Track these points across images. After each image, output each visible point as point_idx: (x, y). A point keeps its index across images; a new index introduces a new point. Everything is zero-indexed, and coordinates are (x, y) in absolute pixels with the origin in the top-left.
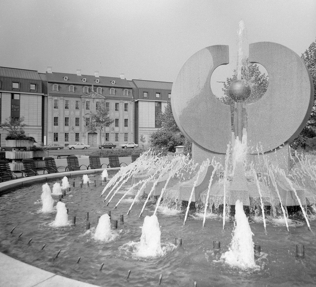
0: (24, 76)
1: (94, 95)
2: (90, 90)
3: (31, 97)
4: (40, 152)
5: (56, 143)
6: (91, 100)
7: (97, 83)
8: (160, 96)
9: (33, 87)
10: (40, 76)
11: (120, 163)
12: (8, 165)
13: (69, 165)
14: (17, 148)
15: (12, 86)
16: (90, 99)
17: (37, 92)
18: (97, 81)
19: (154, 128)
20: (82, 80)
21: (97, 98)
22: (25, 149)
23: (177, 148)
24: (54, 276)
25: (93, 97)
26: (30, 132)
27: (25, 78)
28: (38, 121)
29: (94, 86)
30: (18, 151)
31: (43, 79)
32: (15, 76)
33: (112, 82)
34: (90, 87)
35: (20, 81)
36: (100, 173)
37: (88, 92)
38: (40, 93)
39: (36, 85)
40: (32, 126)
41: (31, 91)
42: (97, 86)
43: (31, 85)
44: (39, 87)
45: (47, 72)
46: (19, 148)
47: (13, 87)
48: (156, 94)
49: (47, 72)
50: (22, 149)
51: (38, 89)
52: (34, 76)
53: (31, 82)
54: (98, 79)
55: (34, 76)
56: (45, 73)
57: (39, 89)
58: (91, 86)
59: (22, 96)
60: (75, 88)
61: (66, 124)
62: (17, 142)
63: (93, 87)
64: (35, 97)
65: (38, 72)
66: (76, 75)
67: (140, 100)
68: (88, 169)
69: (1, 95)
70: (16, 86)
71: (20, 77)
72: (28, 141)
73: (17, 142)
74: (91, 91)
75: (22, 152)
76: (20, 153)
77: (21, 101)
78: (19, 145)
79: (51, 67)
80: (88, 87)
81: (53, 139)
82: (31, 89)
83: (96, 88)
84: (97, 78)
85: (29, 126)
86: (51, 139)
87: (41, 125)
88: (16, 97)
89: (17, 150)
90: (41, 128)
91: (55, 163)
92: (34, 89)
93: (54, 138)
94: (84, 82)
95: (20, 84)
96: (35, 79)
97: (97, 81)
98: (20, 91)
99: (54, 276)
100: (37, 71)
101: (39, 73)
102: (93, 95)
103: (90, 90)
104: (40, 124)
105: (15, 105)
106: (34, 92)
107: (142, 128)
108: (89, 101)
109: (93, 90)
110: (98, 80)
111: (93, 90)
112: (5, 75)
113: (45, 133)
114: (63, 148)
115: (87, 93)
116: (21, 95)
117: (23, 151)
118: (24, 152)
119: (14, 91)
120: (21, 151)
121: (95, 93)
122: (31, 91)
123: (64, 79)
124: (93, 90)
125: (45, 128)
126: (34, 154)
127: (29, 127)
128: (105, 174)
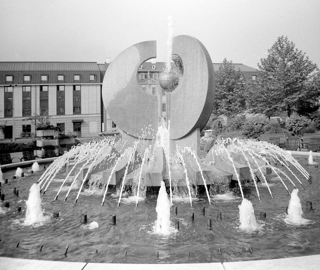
0: (68, 68)
1: (150, 81)
2: (146, 77)
3: (91, 87)
4: (67, 139)
5: (114, 129)
6: (147, 86)
7: (153, 69)
8: (95, 78)
9: (92, 78)
10: (99, 67)
11: (12, 158)
12: (54, 151)
13: (24, 156)
14: (44, 137)
15: (74, 78)
16: (146, 85)
17: (96, 82)
18: (154, 67)
19: (72, 115)
20: (151, 67)
21: (153, 84)
22: (52, 137)
23: (206, 133)
24: (86, 265)
25: (149, 83)
26: (90, 120)
27: (85, 70)
28: (98, 109)
29: (151, 72)
30: (46, 140)
31: (102, 70)
32: (77, 70)
33: (152, 67)
34: (146, 73)
35: (81, 74)
36: (30, 165)
37: (144, 79)
38: (99, 83)
39: (95, 75)
40: (85, 114)
41: (90, 81)
42: (153, 72)
43: (91, 76)
44: (97, 77)
45: (105, 62)
46: (47, 137)
47: (75, 79)
48: (89, 76)
49: (105, 62)
50: (49, 138)
51: (96, 79)
52: (93, 68)
53: (42, 73)
54: (154, 65)
55: (93, 68)
56: (104, 63)
57: (97, 79)
58: (147, 72)
59: (50, 88)
60: (145, 75)
61: (163, 110)
62: (44, 132)
63: (148, 74)
64: (94, 87)
65: (98, 63)
66: (151, 63)
67: (51, 84)
68: (21, 161)
69: (65, 87)
70: (77, 78)
71: (81, 70)
72: (54, 130)
73: (44, 132)
74: (147, 78)
75: (49, 141)
76: (46, 141)
77: (81, 91)
78: (45, 135)
79: (109, 58)
80: (144, 74)
81: (112, 126)
82: (91, 79)
83: (152, 74)
84: (154, 64)
85: (89, 114)
86: (110, 126)
87: (100, 112)
88: (78, 88)
89: (45, 138)
90: (100, 115)
91: (54, 152)
92: (93, 79)
93: (113, 124)
94: (141, 69)
95: (81, 76)
96: (94, 70)
97: (154, 67)
98: (80, 82)
99: (86, 265)
100: (96, 63)
101: (98, 64)
102: (149, 81)
103: (146, 77)
104: (99, 112)
105: (77, 96)
106: (93, 83)
107: (89, 114)
108: (145, 87)
109: (149, 76)
110: (155, 66)
111: (149, 76)
112: (68, 69)
113: (104, 120)
114: (119, 134)
115: (143, 80)
116: (81, 86)
117: (50, 139)
118: (51, 141)
119: (60, 83)
120: (48, 139)
121: (152, 79)
122: (90, 81)
123: (152, 68)
124: (149, 76)
125: (104, 115)
126: (59, 142)
127: (90, 116)
128: (35, 167)
